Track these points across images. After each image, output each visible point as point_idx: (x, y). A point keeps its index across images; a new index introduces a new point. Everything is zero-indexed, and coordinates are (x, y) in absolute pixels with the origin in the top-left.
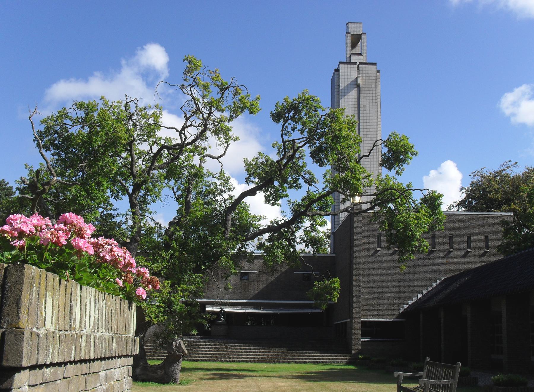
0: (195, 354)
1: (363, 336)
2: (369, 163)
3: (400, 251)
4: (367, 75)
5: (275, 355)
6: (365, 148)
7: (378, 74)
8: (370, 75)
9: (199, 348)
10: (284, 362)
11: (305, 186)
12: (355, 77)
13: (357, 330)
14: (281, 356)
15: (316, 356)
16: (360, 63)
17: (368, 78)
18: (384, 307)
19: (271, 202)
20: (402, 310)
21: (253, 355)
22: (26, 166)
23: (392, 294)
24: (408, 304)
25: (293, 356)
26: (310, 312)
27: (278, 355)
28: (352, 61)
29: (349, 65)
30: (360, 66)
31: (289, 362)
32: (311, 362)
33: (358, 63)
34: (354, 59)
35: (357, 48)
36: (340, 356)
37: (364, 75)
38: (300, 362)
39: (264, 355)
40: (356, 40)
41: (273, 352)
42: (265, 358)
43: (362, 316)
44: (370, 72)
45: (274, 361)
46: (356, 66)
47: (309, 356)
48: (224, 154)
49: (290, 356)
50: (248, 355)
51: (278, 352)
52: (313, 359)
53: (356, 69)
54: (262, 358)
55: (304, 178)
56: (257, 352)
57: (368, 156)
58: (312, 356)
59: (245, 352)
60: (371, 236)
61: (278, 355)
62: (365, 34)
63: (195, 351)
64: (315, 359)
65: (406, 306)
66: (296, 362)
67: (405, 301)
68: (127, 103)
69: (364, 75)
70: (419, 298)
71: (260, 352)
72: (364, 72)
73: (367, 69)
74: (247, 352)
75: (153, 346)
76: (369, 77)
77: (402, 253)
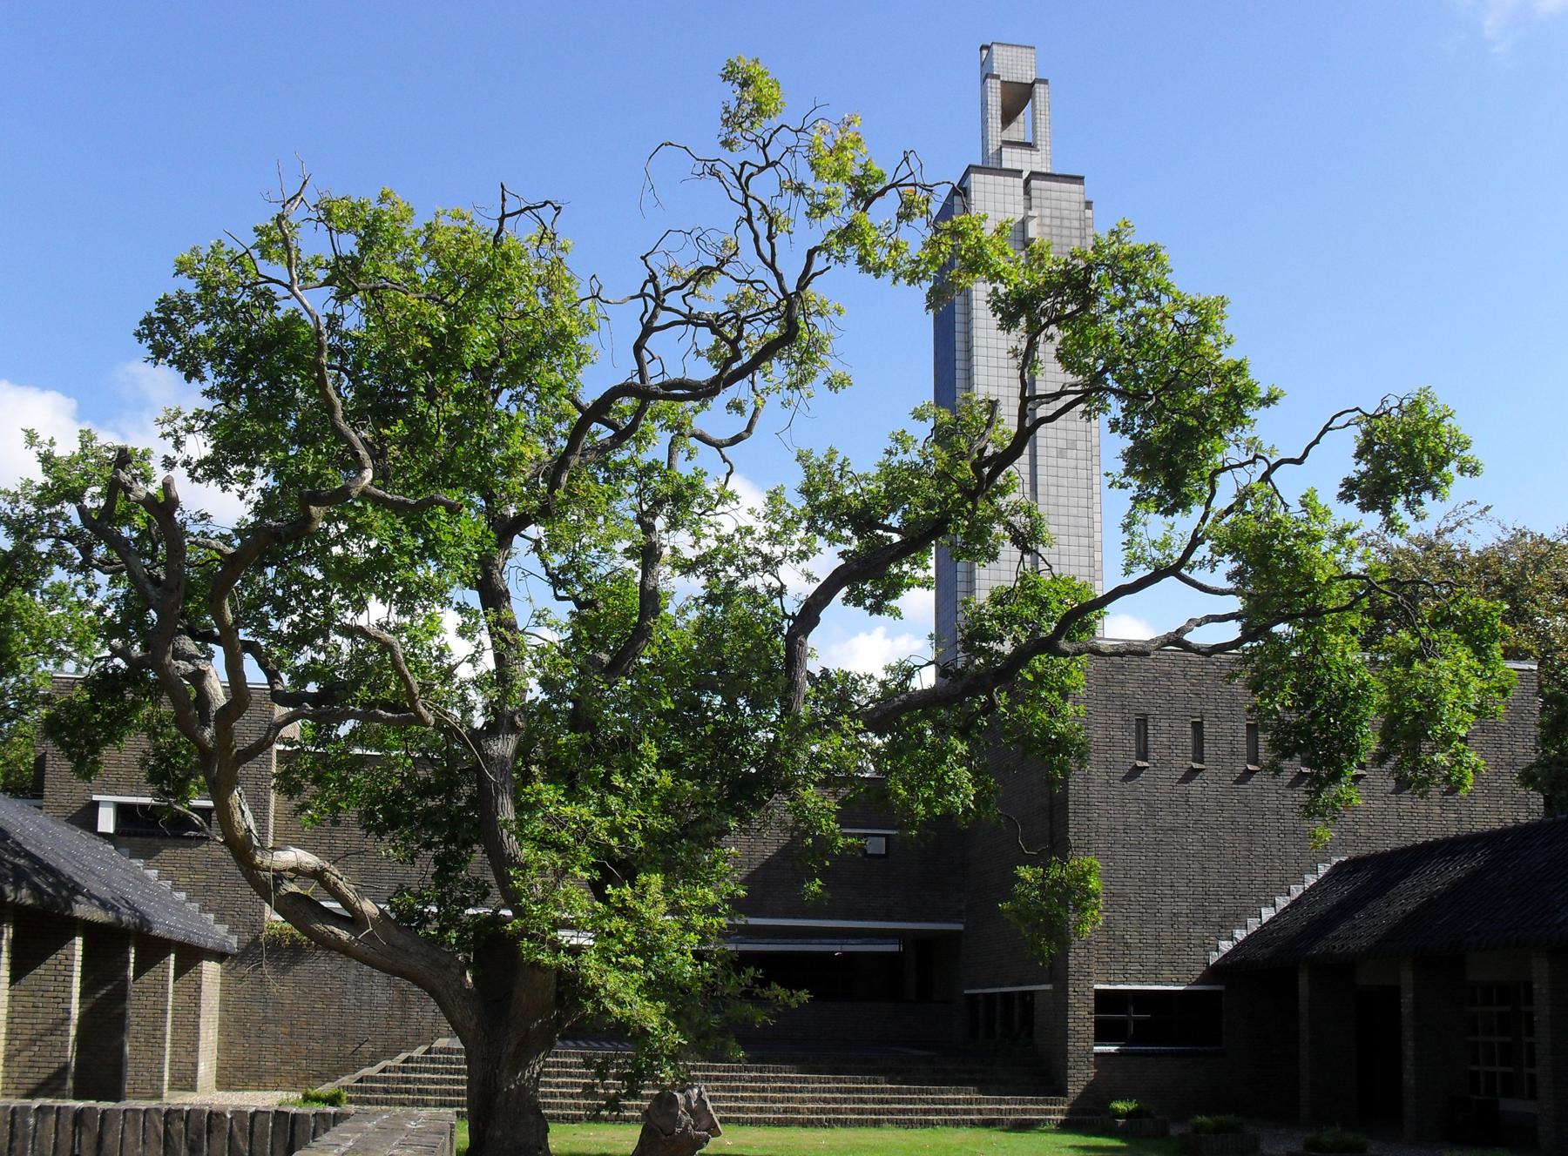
0: (563, 1095)
1: (1100, 1038)
2: (1063, 491)
3: (1315, 779)
4: (1056, 213)
5: (825, 1101)
6: (1051, 443)
7: (1089, 213)
8: (1065, 213)
9: (570, 1075)
10: (860, 1123)
11: (1009, 552)
12: (1019, 218)
13: (1081, 1018)
14: (845, 1101)
15: (955, 1102)
16: (1034, 175)
17: (1057, 222)
18: (1159, 946)
19: (868, 602)
20: (1214, 958)
21: (752, 1099)
22: (31, 437)
23: (1183, 907)
24: (1231, 938)
25: (881, 1101)
26: (837, 949)
27: (835, 1100)
28: (1005, 165)
29: (1000, 179)
30: (1034, 183)
31: (877, 1124)
32: (946, 1123)
33: (1025, 175)
34: (1012, 158)
35: (1014, 125)
36: (1031, 1102)
37: (1047, 212)
38: (911, 1124)
39: (789, 1100)
40: (1017, 98)
41: (814, 1090)
42: (797, 1111)
43: (1095, 977)
44: (1064, 205)
45: (828, 1121)
46: (1020, 182)
47: (934, 1102)
48: (749, 430)
49: (874, 1101)
50: (737, 1099)
51: (830, 1091)
52: (949, 1112)
53: (1021, 191)
54: (785, 1111)
55: (1009, 526)
56: (764, 1090)
57: (1299, 462)
58: (943, 1102)
59: (724, 1089)
60: (1118, 721)
61: (835, 1100)
62: (1045, 82)
63: (557, 1085)
64: (956, 1112)
65: (1226, 946)
66: (899, 1124)
67: (1224, 930)
68: (504, 216)
69: (1047, 212)
70: (1265, 918)
71: (774, 1090)
72: (1046, 203)
73: (1054, 195)
74: (731, 1089)
75: (587, 1107)
76: (1062, 219)
77: (1318, 784)
